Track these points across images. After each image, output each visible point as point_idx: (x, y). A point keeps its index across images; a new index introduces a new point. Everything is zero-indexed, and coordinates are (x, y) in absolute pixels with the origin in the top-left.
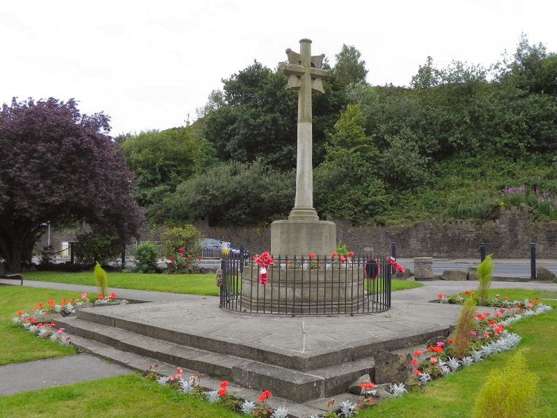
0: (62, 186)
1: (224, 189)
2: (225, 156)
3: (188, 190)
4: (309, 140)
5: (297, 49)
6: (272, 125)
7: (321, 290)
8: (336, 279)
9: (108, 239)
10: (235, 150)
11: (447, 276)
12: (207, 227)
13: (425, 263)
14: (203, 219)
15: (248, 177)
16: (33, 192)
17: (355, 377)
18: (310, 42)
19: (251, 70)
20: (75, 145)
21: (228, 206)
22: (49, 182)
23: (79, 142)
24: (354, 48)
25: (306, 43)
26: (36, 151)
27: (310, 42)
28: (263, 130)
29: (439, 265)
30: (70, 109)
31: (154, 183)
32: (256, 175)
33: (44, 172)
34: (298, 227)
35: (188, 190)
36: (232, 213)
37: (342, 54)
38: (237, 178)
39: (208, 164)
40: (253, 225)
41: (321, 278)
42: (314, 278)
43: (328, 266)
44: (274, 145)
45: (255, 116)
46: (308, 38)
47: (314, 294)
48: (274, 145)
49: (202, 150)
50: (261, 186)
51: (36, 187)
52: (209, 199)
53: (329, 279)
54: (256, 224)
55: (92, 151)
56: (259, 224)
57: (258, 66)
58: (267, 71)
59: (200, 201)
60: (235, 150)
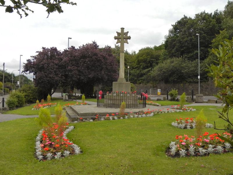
0: (93, 72)
1: (168, 69)
2: (172, 56)
3: (155, 71)
4: (123, 58)
5: (120, 31)
6: (190, 42)
7: (117, 101)
8: (136, 98)
9: (109, 88)
10: (175, 53)
11: (209, 101)
12: (164, 84)
13: (199, 96)
14: (162, 81)
15: (176, 64)
16: (85, 74)
17: (87, 118)
18: (124, 28)
19: (182, 19)
20: (96, 58)
21: (170, 75)
22: (89, 71)
23: (97, 57)
24: (56, 48)
25: (123, 29)
26: (86, 61)
27: (124, 28)
28: (186, 44)
29: (205, 98)
30: (94, 46)
31: (147, 67)
32: (180, 63)
33: (88, 68)
34: (120, 84)
35: (155, 71)
36: (172, 78)
37: (228, 6)
38: (173, 64)
39: (165, 59)
40: (180, 83)
41: (119, 98)
42: (117, 98)
43: (122, 95)
44: (191, 50)
45: (183, 38)
46: (123, 27)
47: (115, 103)
48: (191, 50)
49: (162, 54)
50: (182, 67)
51: (86, 72)
52: (162, 73)
53: (122, 98)
54: (182, 82)
55: (101, 60)
56: (183, 82)
57: (186, 17)
58: (190, 19)
59: (159, 74)
60: (175, 53)
